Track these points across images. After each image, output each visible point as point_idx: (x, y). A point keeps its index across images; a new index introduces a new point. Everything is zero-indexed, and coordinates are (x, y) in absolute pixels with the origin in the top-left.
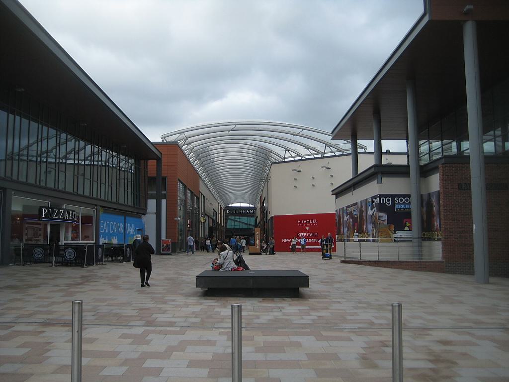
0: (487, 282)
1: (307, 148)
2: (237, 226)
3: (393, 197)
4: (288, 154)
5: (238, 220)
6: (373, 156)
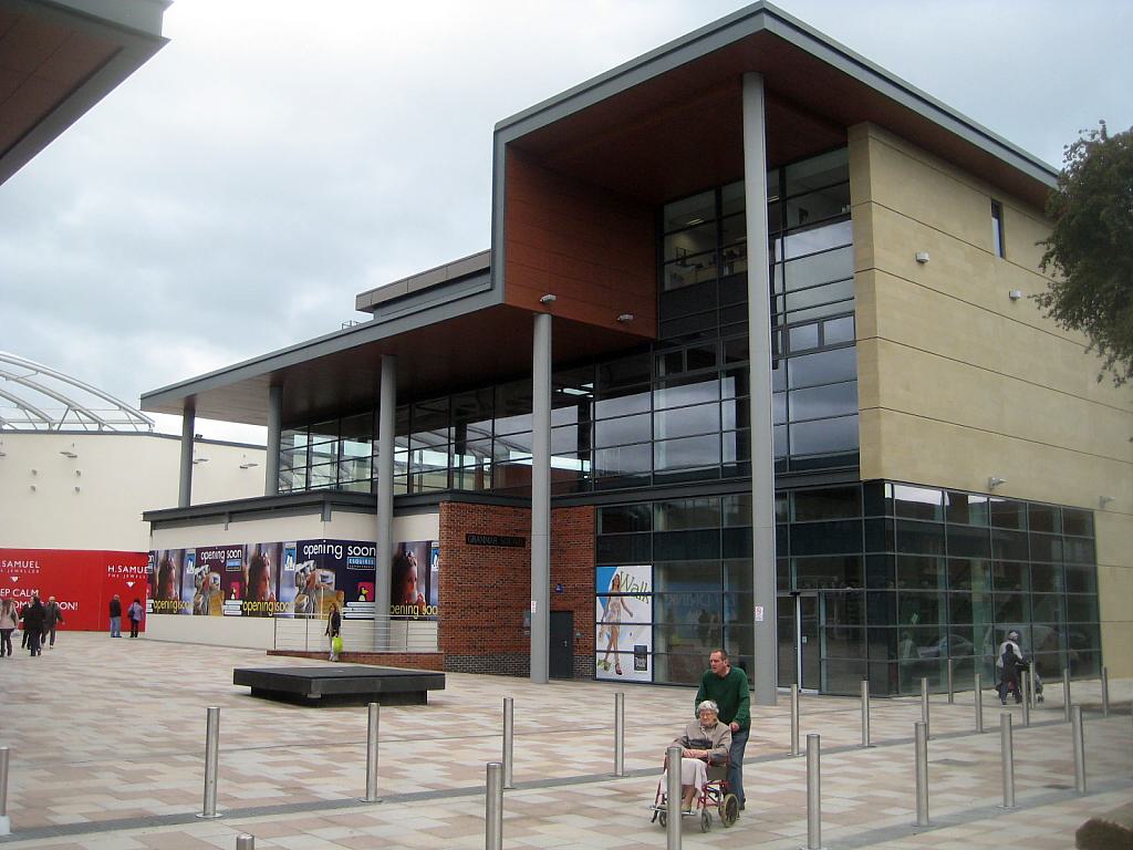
0: (547, 683)
1: (21, 406)
3: (345, 544)
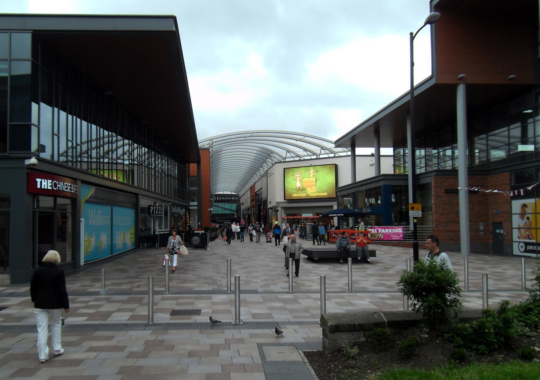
1: (305, 150)
2: (220, 211)
4: (288, 155)
5: (221, 206)
6: (350, 158)
